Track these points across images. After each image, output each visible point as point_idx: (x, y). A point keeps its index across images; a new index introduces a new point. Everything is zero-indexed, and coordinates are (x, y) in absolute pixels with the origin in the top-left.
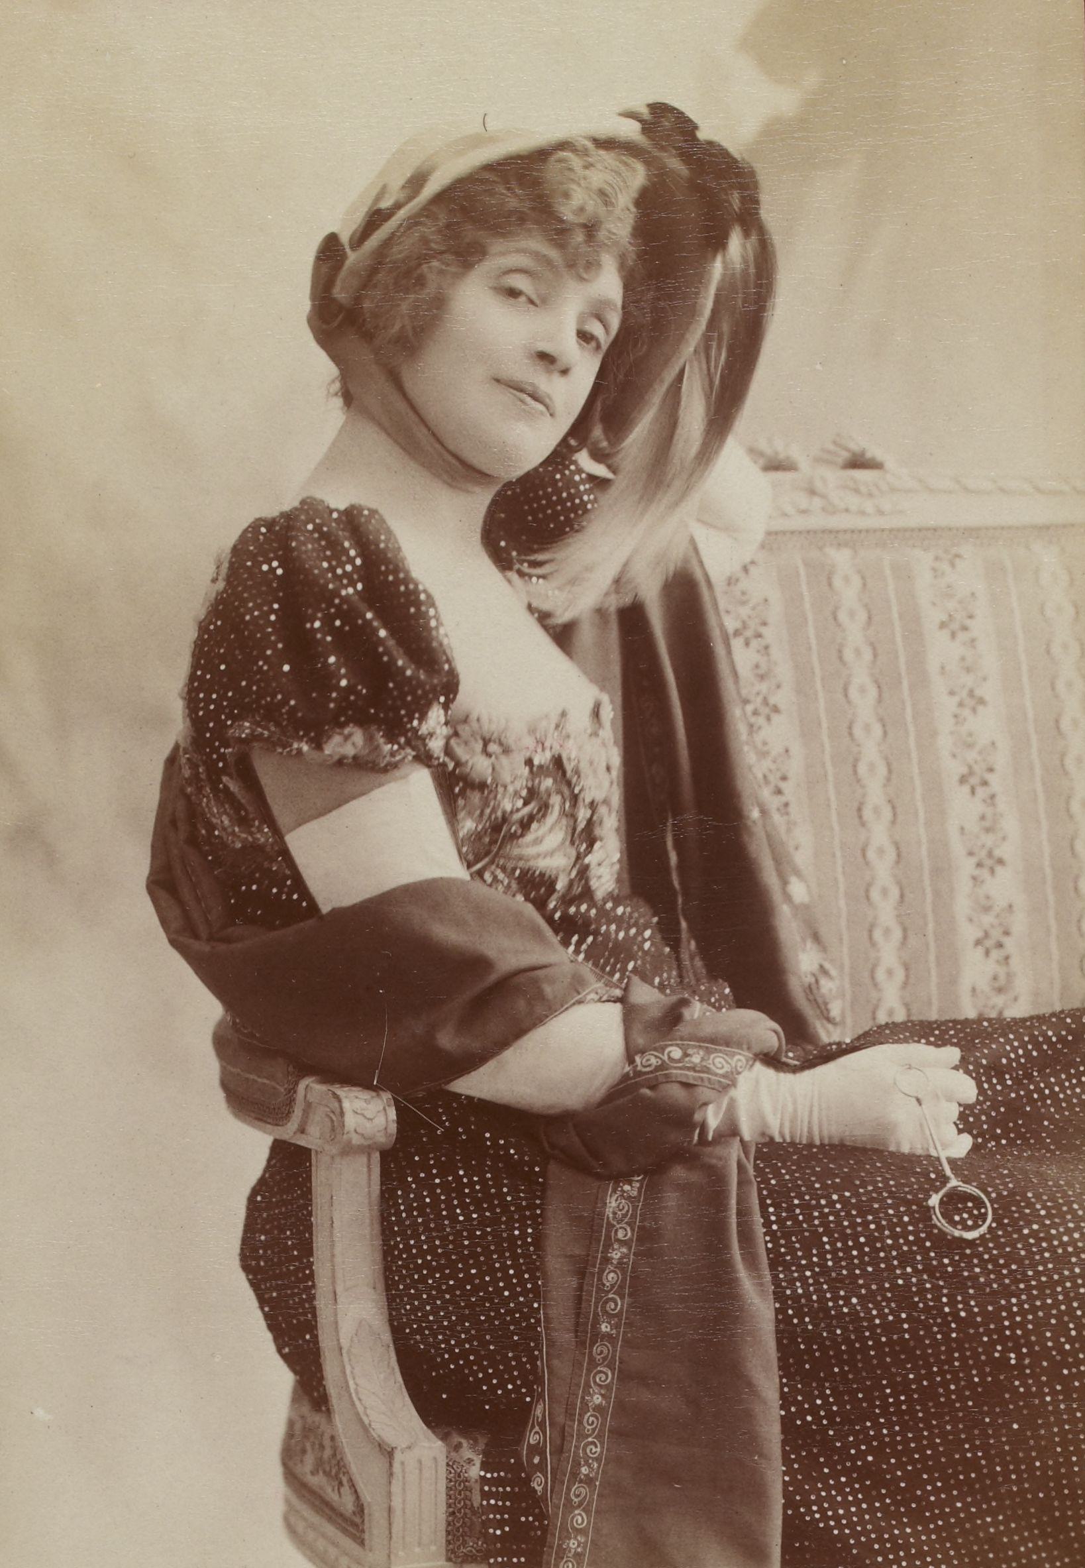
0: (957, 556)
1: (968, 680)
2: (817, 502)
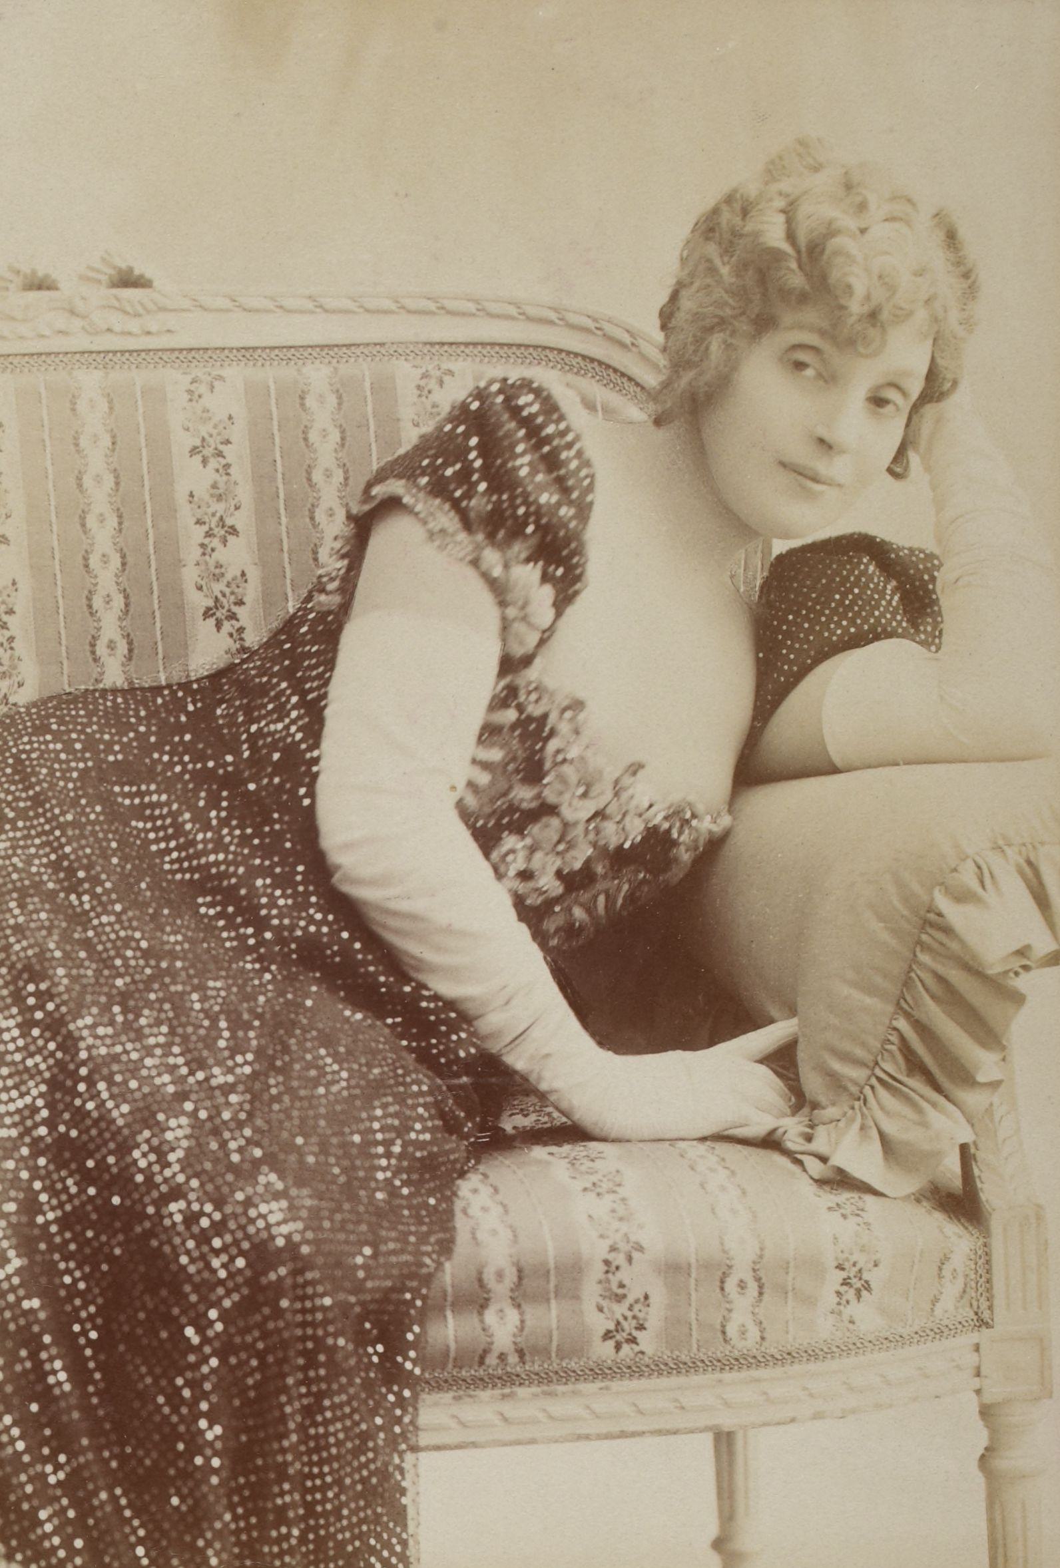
0: (221, 378)
1: (220, 508)
2: (77, 323)
